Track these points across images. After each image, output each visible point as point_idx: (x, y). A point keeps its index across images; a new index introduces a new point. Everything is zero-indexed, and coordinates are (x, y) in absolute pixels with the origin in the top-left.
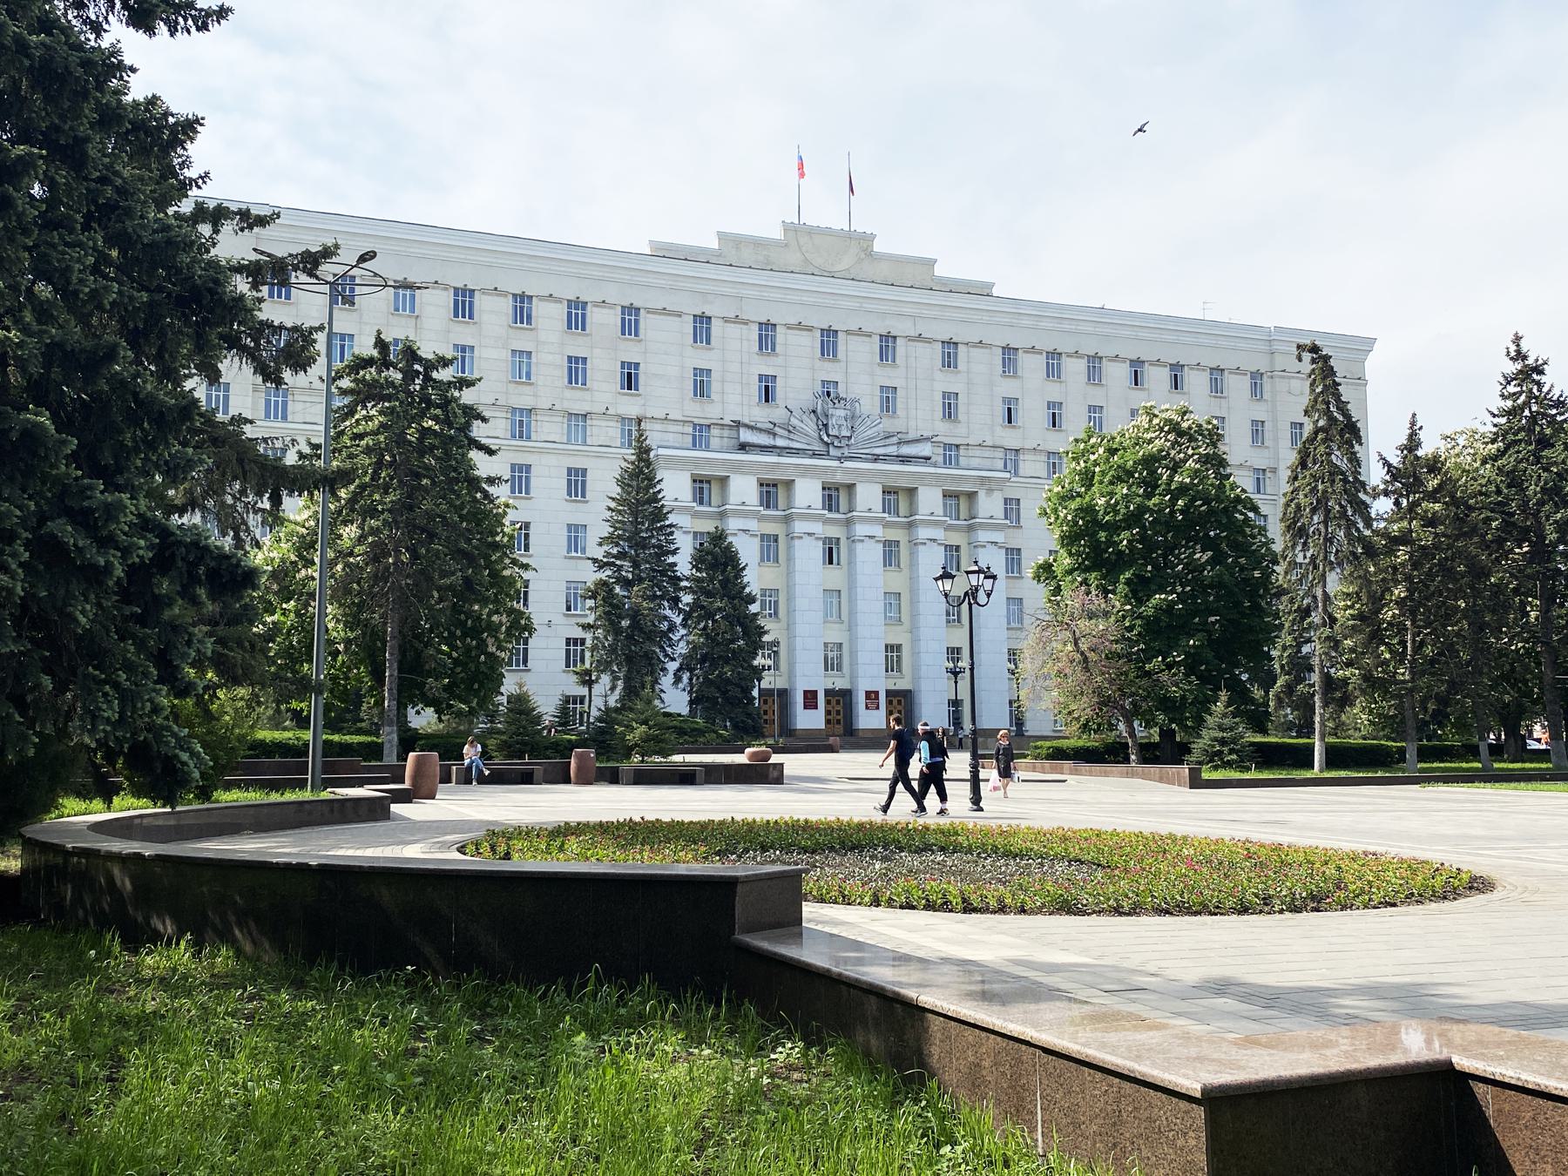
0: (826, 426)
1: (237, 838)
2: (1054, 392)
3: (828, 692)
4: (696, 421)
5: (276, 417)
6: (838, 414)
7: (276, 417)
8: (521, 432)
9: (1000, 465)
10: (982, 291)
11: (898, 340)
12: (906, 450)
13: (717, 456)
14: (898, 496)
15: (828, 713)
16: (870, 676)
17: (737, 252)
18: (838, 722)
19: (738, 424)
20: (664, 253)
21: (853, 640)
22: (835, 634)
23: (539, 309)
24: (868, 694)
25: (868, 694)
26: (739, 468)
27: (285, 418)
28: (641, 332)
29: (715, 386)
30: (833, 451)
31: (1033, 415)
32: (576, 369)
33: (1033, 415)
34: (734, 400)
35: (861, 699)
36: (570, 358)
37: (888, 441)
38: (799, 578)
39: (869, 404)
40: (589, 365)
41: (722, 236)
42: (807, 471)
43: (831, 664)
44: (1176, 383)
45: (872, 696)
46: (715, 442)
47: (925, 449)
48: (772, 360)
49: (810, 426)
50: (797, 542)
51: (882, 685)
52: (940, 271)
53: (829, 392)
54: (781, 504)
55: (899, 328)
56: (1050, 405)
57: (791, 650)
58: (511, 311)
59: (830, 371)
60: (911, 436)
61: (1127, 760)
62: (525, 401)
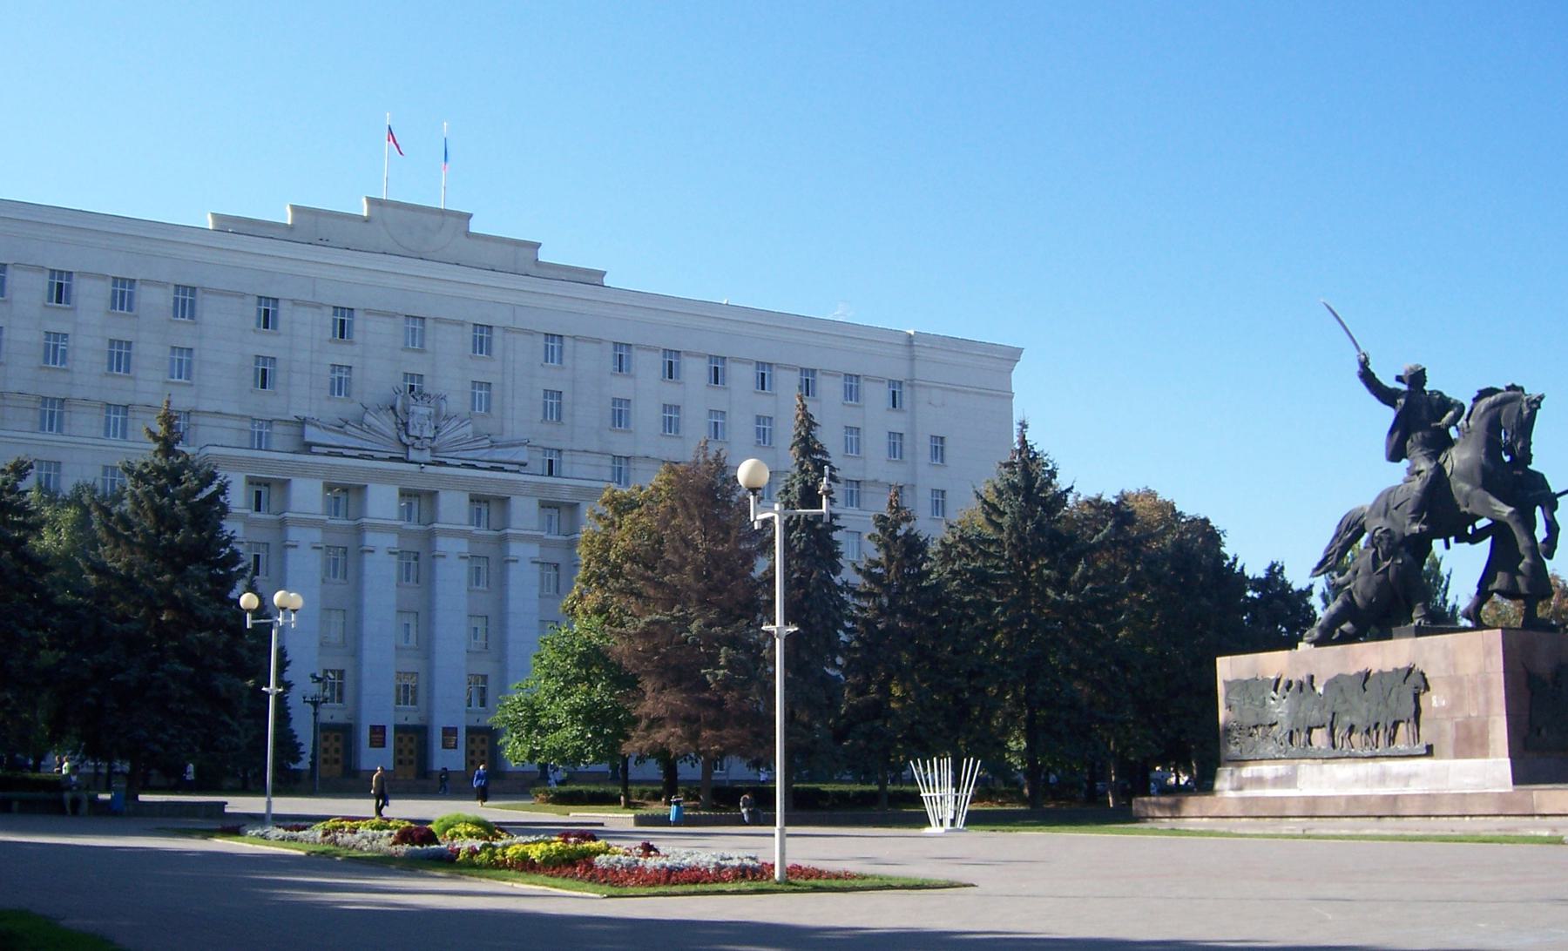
0: (406, 425)
1: (558, 881)
2: (671, 393)
3: (399, 729)
4: (256, 416)
5: (51, 429)
6: (421, 410)
7: (51, 429)
8: (406, 698)
9: (607, 474)
10: (592, 278)
11: (281, 303)
12: (499, 455)
13: (277, 457)
14: (488, 505)
15: (398, 751)
16: (450, 709)
17: (314, 227)
18: (337, 761)
19: (302, 422)
20: (225, 224)
21: (358, 667)
22: (485, 667)
23: (867, 389)
24: (373, 729)
25: (373, 729)
26: (305, 472)
27: (124, 436)
28: (198, 314)
29: (280, 378)
30: (413, 455)
31: (647, 415)
32: (120, 356)
33: (647, 415)
34: (302, 395)
35: (365, 735)
36: (112, 342)
37: (481, 444)
38: (368, 599)
39: (457, 402)
40: (134, 350)
41: (296, 210)
42: (384, 477)
43: (406, 694)
44: (670, 371)
45: (378, 733)
46: (276, 442)
47: (522, 455)
48: (346, 348)
49: (386, 424)
50: (367, 555)
51: (461, 722)
52: (544, 256)
53: (414, 388)
54: (274, 508)
55: (497, 318)
56: (667, 408)
57: (358, 682)
58: (109, 295)
59: (416, 364)
60: (506, 437)
61: (619, 802)
62: (56, 390)
